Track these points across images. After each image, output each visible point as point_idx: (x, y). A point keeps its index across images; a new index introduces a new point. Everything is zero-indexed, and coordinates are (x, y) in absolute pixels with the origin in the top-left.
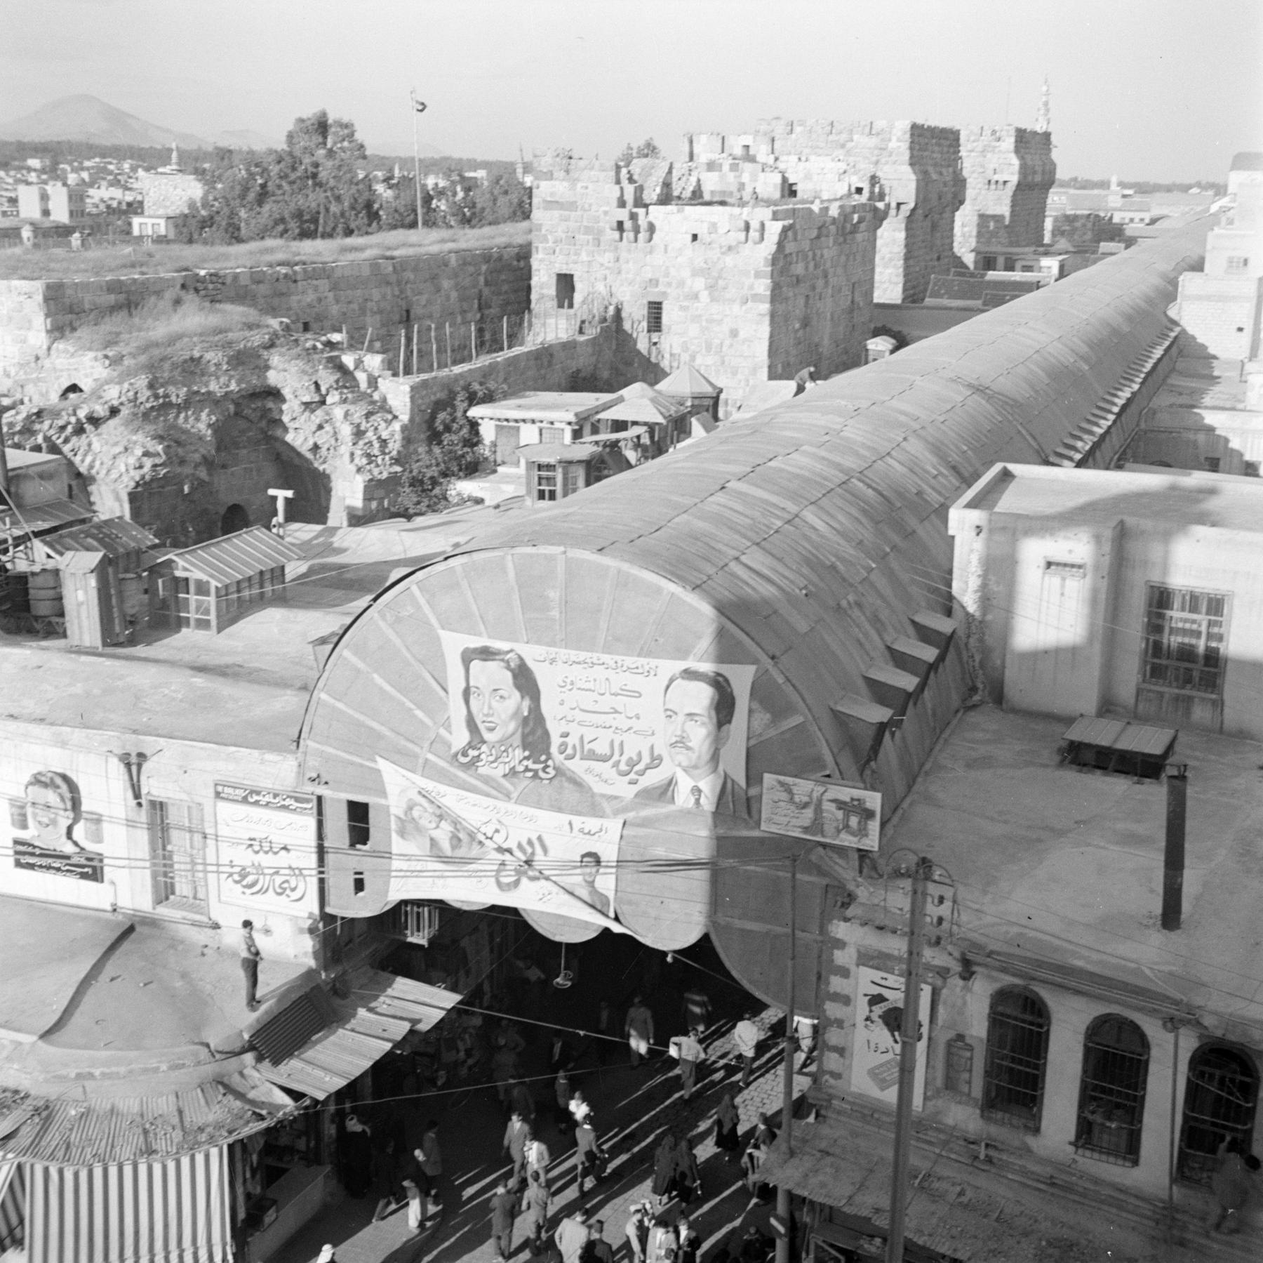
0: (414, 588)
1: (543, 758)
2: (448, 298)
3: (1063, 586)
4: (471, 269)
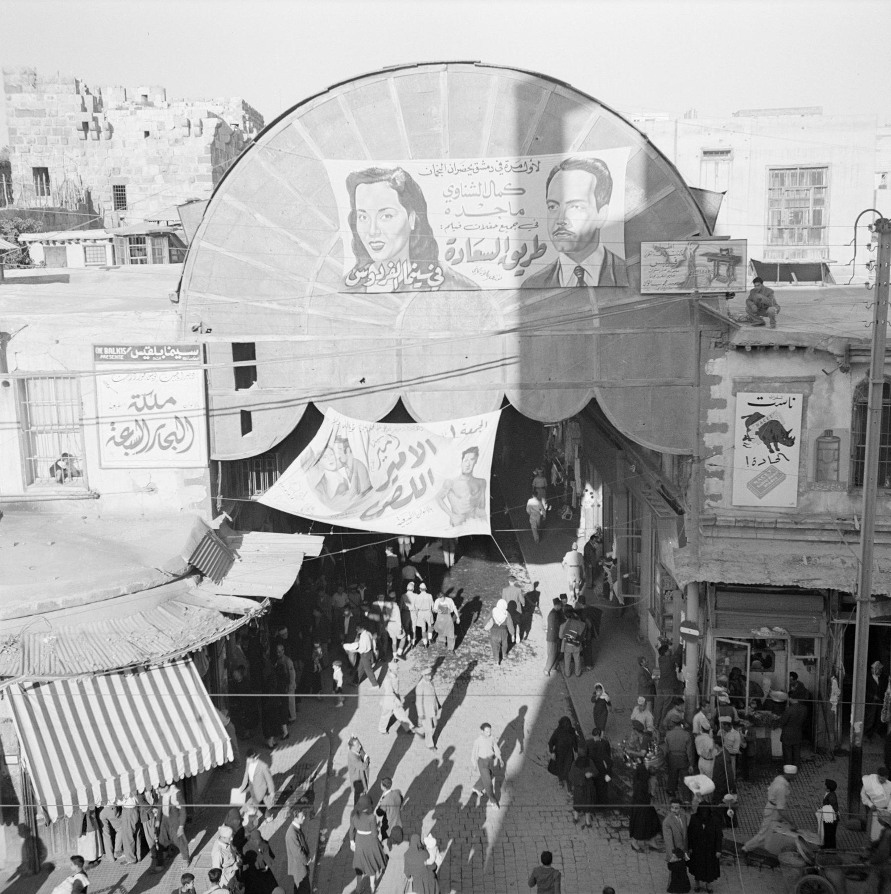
1: (431, 267)
3: (716, 170)
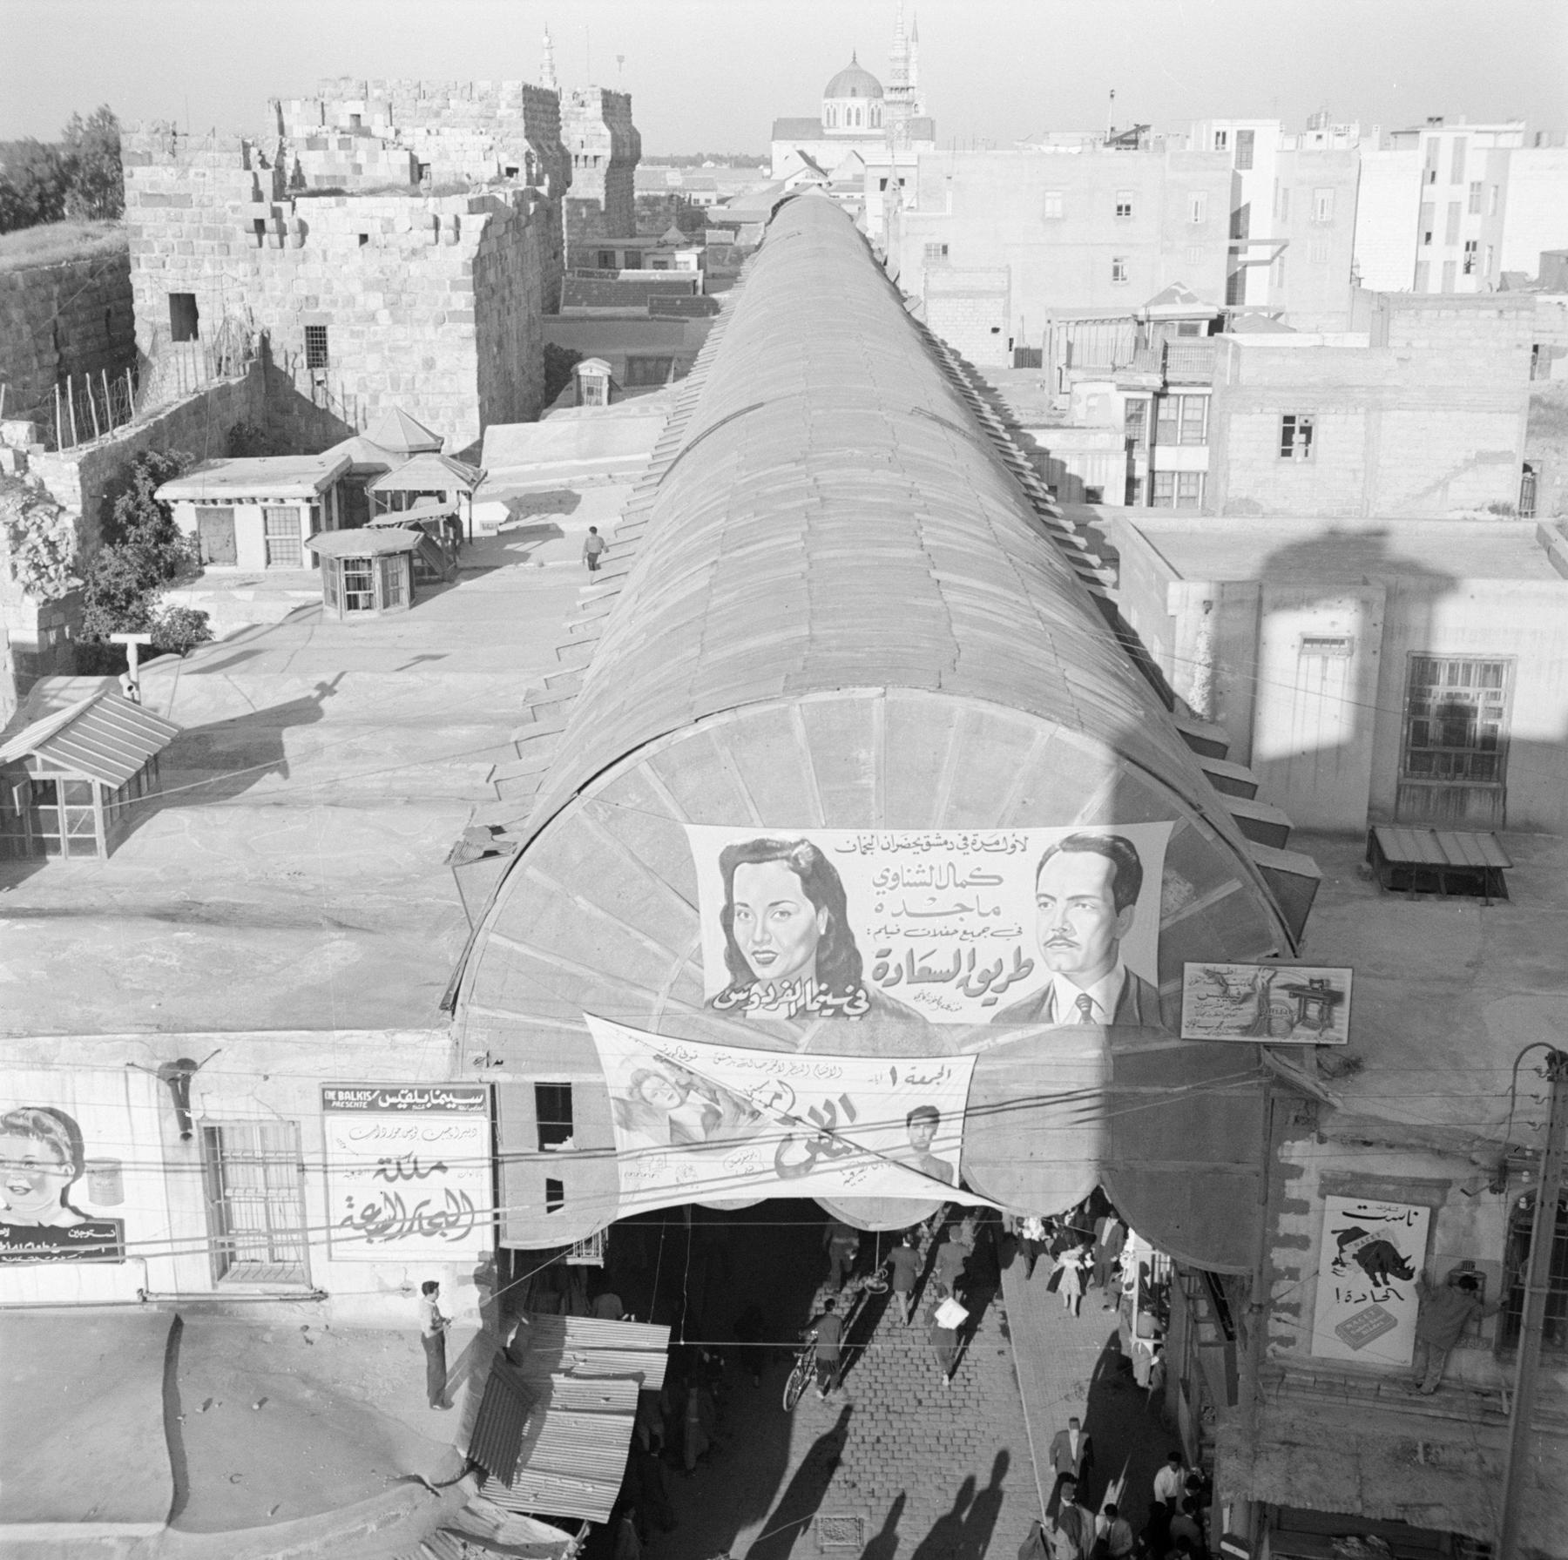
0: (644, 768)
1: (850, 989)
2: (19, 332)
3: (1324, 668)
4: (43, 292)
